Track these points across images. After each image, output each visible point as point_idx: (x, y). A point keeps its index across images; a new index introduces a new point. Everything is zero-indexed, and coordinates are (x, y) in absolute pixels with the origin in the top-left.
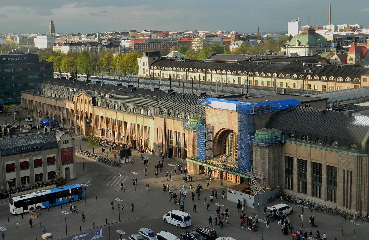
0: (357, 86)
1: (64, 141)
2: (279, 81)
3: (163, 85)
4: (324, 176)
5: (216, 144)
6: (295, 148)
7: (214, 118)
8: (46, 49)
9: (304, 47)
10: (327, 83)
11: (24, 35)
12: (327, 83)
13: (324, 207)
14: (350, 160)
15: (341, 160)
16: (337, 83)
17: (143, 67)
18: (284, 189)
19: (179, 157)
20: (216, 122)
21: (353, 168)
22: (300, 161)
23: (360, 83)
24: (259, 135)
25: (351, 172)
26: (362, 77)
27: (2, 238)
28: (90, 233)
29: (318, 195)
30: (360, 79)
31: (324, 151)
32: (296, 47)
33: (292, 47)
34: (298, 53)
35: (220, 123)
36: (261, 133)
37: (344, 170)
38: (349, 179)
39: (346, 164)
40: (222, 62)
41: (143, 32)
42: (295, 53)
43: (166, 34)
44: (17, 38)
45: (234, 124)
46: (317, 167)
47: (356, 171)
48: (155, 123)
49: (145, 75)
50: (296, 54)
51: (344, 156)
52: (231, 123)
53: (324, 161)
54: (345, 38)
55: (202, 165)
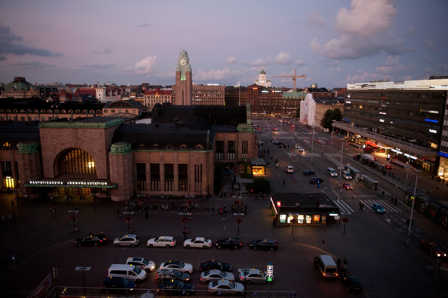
0: (99, 116)
2: (19, 116)
4: (176, 172)
5: (56, 165)
6: (148, 155)
7: (53, 140)
9: (19, 92)
10: (186, 104)
12: (186, 104)
13: (379, 160)
14: (200, 156)
15: (192, 158)
20: (57, 143)
21: (203, 162)
22: (152, 165)
23: (102, 114)
24: (119, 149)
25: (201, 165)
26: (103, 109)
28: (43, 286)
30: (102, 111)
31: (176, 154)
32: (12, 92)
33: (8, 92)
34: (13, 97)
35: (63, 144)
36: (120, 146)
37: (195, 165)
38: (200, 170)
39: (197, 160)
40: (213, 86)
42: (11, 97)
45: (82, 143)
47: (205, 163)
50: (12, 97)
51: (195, 154)
52: (78, 142)
53: (176, 161)
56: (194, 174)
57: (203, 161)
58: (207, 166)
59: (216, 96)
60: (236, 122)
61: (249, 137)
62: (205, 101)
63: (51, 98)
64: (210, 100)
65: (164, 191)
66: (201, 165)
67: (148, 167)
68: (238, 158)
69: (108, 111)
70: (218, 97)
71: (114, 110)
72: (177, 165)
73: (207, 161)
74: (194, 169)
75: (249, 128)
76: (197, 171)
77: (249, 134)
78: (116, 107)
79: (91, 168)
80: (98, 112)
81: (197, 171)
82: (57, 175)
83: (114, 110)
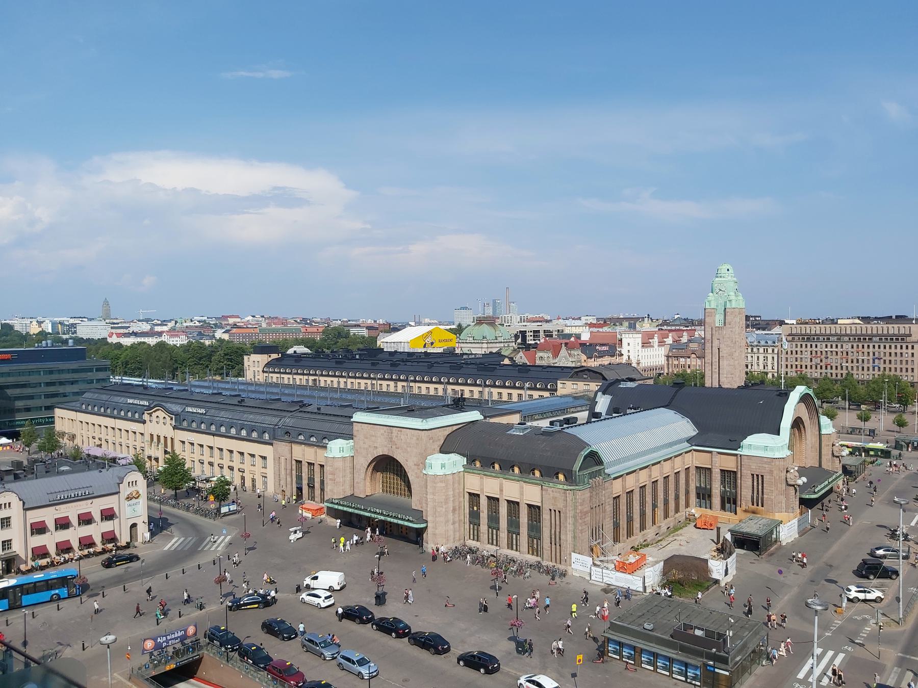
1: (129, 483)
3: (286, 394)
8: (16, 412)
11: (60, 319)
16: (838, 323)
17: (252, 369)
18: (467, 540)
19: (757, 475)
27: (27, 639)
29: (514, 547)
32: (470, 341)
37: (763, 506)
41: (250, 318)
43: (284, 322)
44: (49, 324)
46: (513, 505)
48: (275, 451)
49: (256, 380)
54: (531, 332)
55: (348, 510)
61: (766, 466)
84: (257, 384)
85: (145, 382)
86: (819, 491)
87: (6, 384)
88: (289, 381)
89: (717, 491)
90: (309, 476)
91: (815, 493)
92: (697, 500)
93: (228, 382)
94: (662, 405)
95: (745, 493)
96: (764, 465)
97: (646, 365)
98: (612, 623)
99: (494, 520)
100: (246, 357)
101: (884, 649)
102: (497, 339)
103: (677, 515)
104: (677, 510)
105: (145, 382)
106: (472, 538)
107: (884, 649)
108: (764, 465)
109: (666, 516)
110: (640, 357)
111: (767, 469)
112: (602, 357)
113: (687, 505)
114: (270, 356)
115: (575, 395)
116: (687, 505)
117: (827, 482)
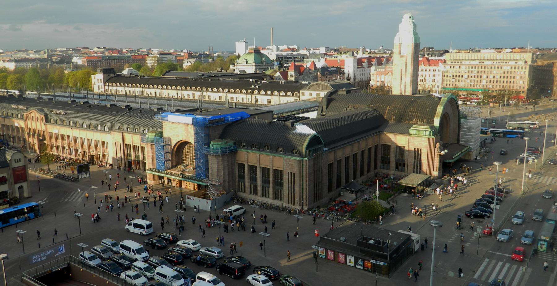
2: (230, 96)
13: (272, 205)
14: (293, 163)
21: (295, 170)
24: (214, 146)
26: (301, 92)
30: (299, 93)
37: (289, 173)
43: (120, 52)
46: (265, 171)
47: (298, 172)
51: (288, 160)
53: (271, 165)
54: (286, 58)
56: (287, 183)
57: (295, 170)
58: (301, 176)
59: (512, 68)
60: (420, 121)
61: (423, 143)
62: (507, 77)
63: (294, 72)
64: (506, 75)
65: (261, 196)
66: (294, 174)
67: (247, 168)
68: (408, 171)
69: (305, 94)
70: (513, 70)
71: (320, 94)
72: (272, 170)
73: (300, 169)
74: (287, 177)
75: (426, 131)
76: (290, 179)
77: (423, 139)
78: (315, 89)
79: (414, 152)
80: (295, 95)
81: (290, 179)
82: (174, 165)
83: (304, 93)
84: (118, 96)
85: (97, 99)
86: (455, 158)
87: (398, 153)
88: (194, 97)
89: (425, 162)
90: (252, 175)
91: (453, 159)
92: (382, 164)
93: (81, 93)
94: (457, 111)
95: (410, 160)
96: (422, 143)
97: (361, 80)
98: (321, 238)
99: (266, 181)
100: (92, 76)
101: (501, 254)
102: (262, 63)
103: (369, 174)
104: (369, 171)
105: (97, 99)
106: (240, 190)
107: (501, 254)
108: (422, 143)
109: (362, 174)
110: (356, 75)
111: (424, 145)
112: (331, 75)
113: (375, 168)
114: (109, 76)
115: (311, 100)
116: (375, 168)
117: (461, 152)
